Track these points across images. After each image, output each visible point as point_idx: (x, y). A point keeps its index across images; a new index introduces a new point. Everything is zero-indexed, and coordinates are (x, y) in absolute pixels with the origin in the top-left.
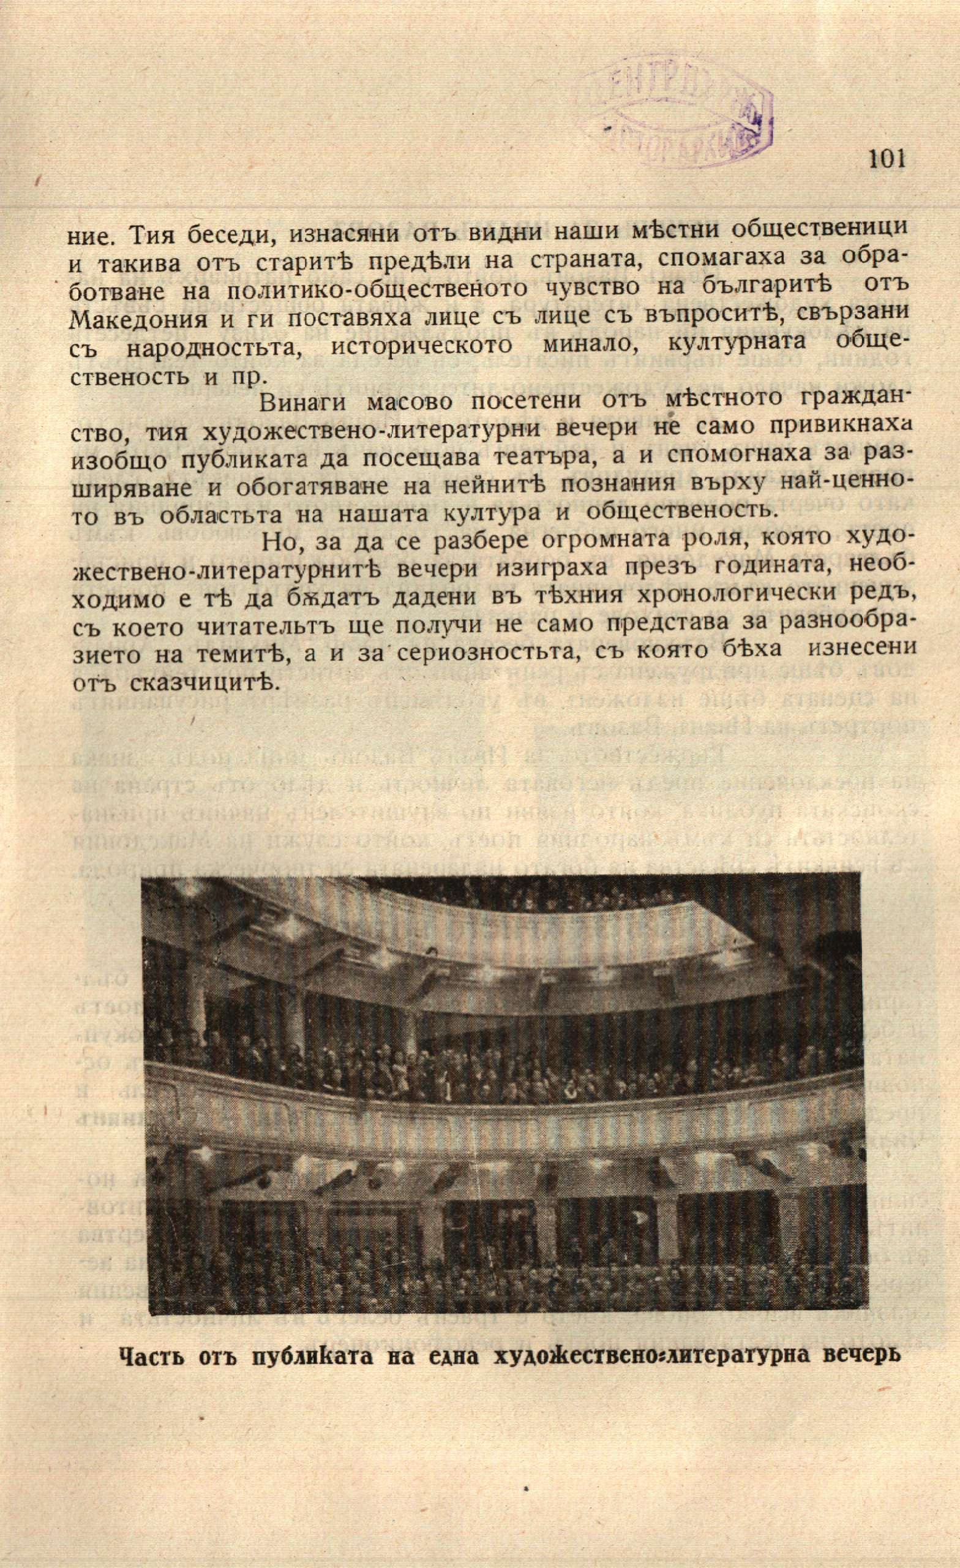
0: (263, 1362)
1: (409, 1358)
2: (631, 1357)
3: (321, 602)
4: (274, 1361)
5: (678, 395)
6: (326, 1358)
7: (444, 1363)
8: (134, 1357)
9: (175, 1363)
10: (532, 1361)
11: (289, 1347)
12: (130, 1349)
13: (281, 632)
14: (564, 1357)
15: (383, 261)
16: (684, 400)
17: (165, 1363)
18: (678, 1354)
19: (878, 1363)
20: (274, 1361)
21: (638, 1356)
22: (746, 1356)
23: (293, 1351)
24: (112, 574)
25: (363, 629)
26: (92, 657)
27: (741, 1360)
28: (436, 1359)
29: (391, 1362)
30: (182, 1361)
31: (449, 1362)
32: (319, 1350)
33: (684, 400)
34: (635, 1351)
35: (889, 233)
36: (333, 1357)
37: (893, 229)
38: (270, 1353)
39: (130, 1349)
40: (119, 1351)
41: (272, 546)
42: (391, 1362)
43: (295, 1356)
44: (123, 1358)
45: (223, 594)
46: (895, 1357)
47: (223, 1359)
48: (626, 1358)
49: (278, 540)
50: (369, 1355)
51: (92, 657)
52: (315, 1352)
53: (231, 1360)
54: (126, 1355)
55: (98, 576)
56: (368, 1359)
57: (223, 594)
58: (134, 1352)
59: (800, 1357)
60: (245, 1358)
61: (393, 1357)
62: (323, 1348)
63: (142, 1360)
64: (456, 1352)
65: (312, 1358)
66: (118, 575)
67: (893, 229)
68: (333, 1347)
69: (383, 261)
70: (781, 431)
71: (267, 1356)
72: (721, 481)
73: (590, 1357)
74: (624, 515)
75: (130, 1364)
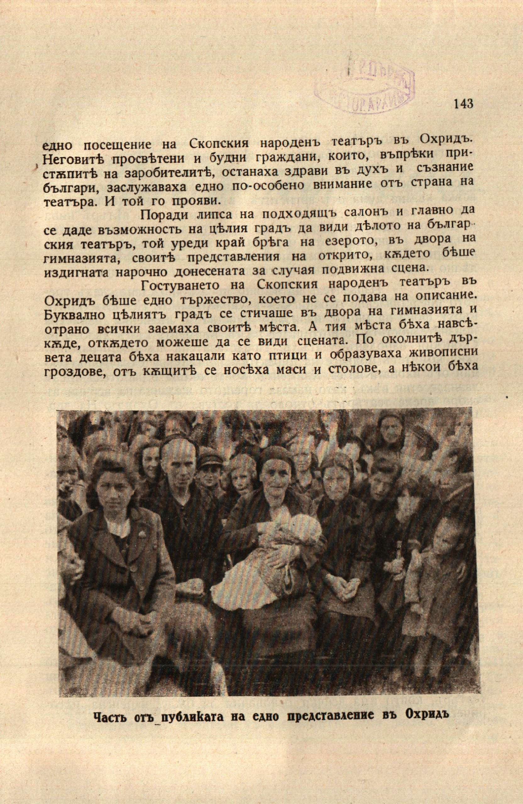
0: (167, 720)
1: (386, 715)
2: (353, 716)
3: (120, 345)
4: (172, 719)
5: (266, 326)
6: (200, 718)
7: (260, 720)
8: (101, 718)
9: (122, 721)
10: (313, 719)
11: (180, 712)
12: (99, 713)
13: (128, 190)
14: (201, 718)
15: (195, 257)
16: (269, 328)
17: (117, 721)
18: (189, 717)
19: (423, 719)
20: (172, 719)
21: (357, 716)
22: (211, 717)
23: (182, 714)
24: (224, 300)
25: (119, 147)
26: (464, 167)
27: (209, 720)
28: (256, 717)
29: (233, 720)
30: (448, 715)
31: (264, 719)
32: (197, 714)
33: (269, 328)
34: (355, 713)
35: (170, 374)
36: (204, 717)
37: (172, 372)
38: (170, 715)
39: (99, 713)
40: (93, 715)
41: (48, 162)
42: (233, 720)
43: (183, 717)
44: (95, 718)
45: (246, 325)
46: (446, 715)
47: (146, 719)
48: (306, 717)
49: (51, 159)
50: (222, 716)
51: (464, 167)
52: (195, 715)
53: (151, 719)
54: (446, 715)
55: (217, 301)
56: (221, 718)
57: (246, 325)
58: (101, 715)
59: (240, 718)
60: (249, 717)
61: (242, 717)
62: (199, 712)
63: (106, 719)
64: (267, 714)
65: (193, 718)
66: (226, 300)
67: (172, 372)
68: (204, 712)
69: (195, 257)
70: (118, 163)
71: (169, 717)
72: (196, 300)
73: (319, 716)
74: (126, 300)
75: (99, 721)
